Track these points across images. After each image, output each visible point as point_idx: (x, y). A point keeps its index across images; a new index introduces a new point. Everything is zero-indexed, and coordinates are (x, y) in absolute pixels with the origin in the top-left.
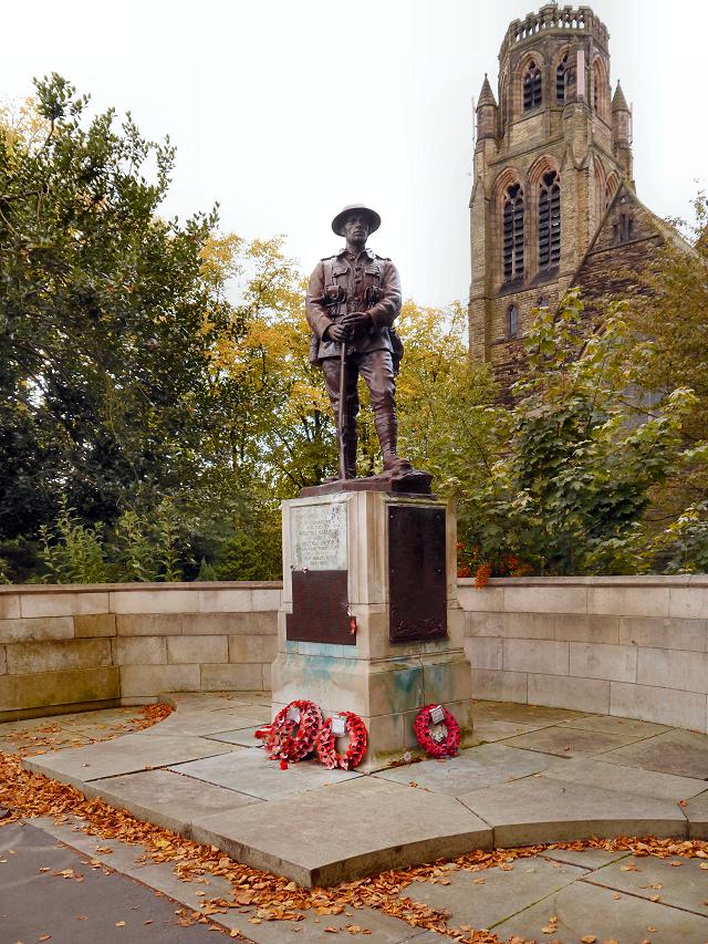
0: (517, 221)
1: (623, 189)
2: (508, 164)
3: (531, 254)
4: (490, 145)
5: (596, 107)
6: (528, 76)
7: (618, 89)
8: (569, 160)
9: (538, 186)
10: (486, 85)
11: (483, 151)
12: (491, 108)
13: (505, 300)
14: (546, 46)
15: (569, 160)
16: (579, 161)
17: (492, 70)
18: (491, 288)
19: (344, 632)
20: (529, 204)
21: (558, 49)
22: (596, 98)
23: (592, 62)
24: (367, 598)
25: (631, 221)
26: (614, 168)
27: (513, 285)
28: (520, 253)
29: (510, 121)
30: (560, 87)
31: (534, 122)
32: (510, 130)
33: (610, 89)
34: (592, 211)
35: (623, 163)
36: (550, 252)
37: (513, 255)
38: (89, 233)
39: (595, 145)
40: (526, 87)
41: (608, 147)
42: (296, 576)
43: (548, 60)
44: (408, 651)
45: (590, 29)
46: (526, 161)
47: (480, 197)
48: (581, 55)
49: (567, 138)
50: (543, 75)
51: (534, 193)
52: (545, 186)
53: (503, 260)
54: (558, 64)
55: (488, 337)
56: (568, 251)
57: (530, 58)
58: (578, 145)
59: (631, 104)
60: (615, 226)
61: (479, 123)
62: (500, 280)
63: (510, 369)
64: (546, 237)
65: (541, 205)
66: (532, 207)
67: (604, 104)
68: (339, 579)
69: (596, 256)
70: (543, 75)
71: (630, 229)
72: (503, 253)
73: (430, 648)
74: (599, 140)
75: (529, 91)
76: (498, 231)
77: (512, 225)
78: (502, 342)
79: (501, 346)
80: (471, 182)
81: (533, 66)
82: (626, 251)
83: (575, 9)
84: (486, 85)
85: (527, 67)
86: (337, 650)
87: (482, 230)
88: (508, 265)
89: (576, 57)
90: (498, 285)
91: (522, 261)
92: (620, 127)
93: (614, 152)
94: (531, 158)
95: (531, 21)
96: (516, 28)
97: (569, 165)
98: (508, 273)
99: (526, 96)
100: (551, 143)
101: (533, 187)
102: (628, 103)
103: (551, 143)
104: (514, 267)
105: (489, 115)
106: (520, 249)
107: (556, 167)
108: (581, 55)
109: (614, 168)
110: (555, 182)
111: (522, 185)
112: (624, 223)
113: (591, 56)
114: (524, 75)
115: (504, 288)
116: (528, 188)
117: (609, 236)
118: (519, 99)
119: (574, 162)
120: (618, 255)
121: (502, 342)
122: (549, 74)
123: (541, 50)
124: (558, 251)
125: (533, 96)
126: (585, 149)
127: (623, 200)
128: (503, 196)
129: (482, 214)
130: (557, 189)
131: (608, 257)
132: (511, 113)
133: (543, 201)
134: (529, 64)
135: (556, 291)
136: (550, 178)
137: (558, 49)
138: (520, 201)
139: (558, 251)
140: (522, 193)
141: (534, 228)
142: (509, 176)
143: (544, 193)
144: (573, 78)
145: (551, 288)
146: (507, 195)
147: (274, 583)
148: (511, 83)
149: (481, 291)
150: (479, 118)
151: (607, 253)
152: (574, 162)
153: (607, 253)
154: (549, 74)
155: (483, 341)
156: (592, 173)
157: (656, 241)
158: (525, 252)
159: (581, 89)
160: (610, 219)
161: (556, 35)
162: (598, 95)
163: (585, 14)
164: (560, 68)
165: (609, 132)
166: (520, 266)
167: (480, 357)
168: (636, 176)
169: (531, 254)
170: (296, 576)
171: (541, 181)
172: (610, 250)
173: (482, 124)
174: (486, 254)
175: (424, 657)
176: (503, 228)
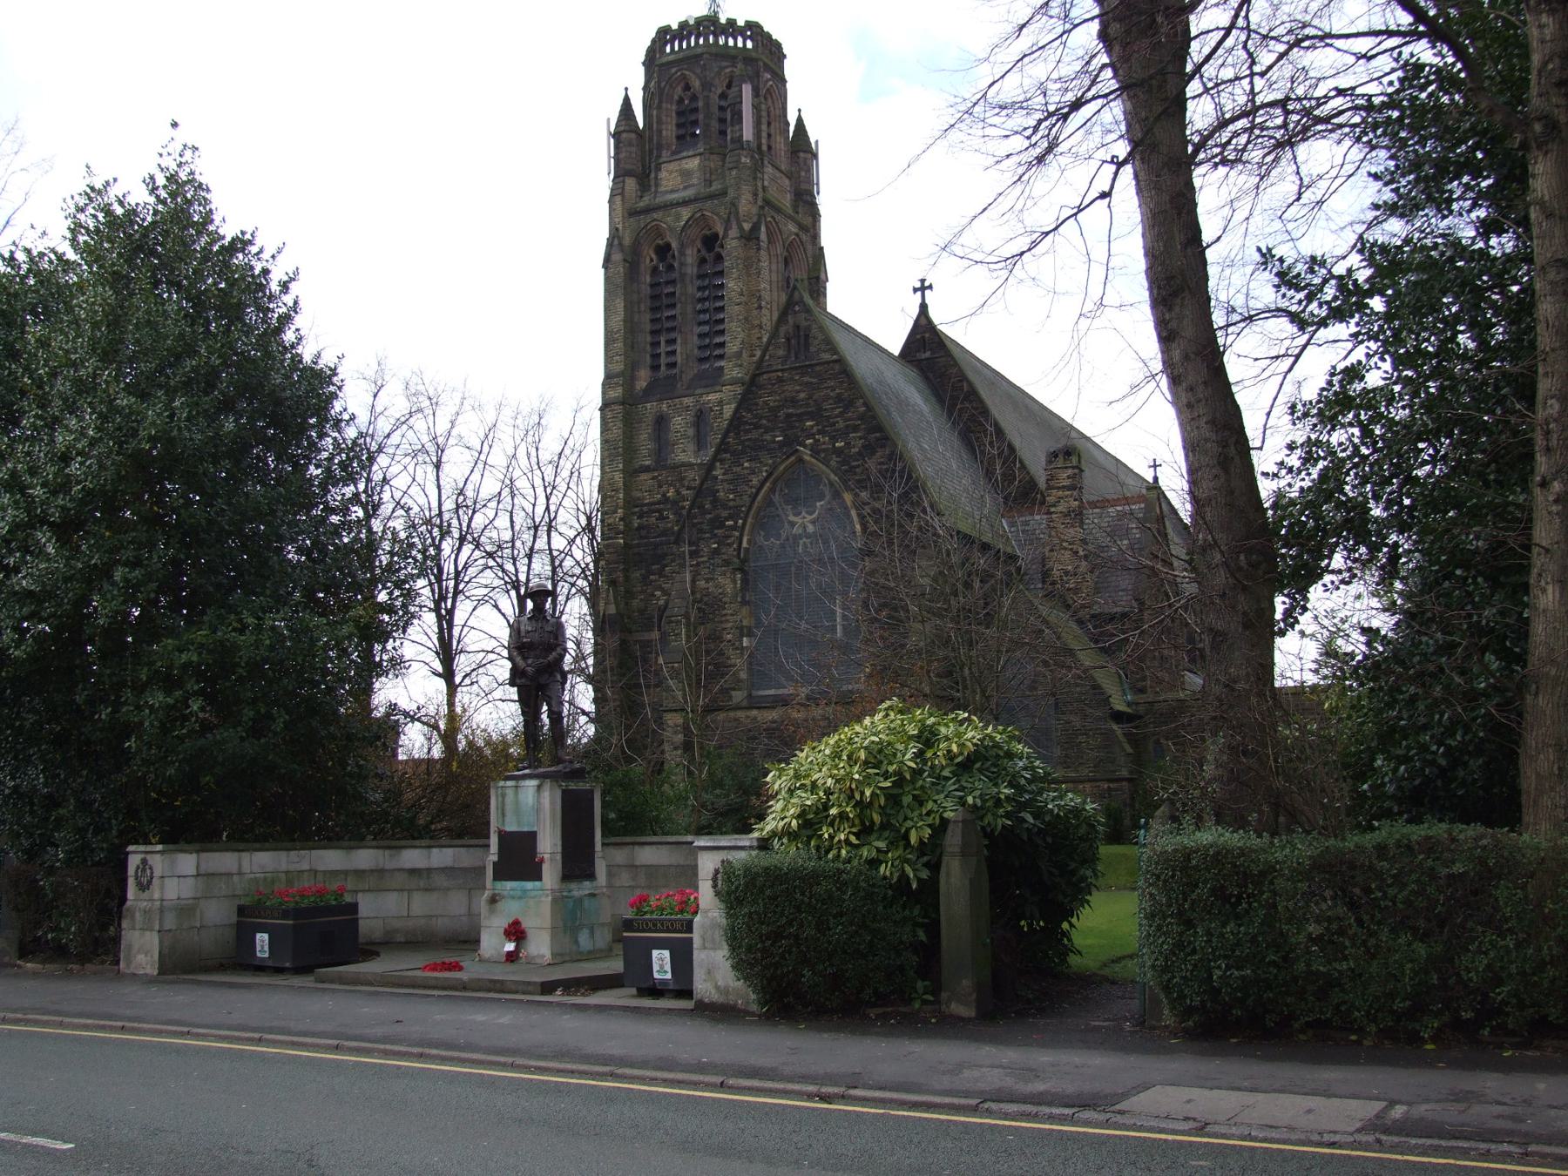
0: (668, 295)
1: (796, 293)
2: (655, 215)
3: (686, 347)
4: (631, 184)
5: (770, 148)
6: (681, 100)
7: (800, 121)
8: (734, 226)
9: (695, 250)
10: (627, 104)
11: (622, 194)
12: (633, 136)
13: (651, 408)
14: (704, 68)
15: (734, 226)
16: (747, 226)
17: (635, 81)
18: (632, 386)
19: (532, 871)
20: (683, 275)
21: (719, 73)
22: (769, 136)
23: (763, 92)
24: (549, 845)
25: (807, 336)
26: (796, 230)
27: (663, 387)
28: (672, 342)
29: (659, 156)
30: (722, 121)
31: (693, 164)
32: (658, 169)
33: (788, 124)
34: (766, 295)
35: (808, 221)
36: (711, 349)
37: (663, 343)
38: (282, 549)
39: (767, 202)
40: (679, 114)
41: (786, 201)
42: (503, 836)
43: (707, 85)
44: (573, 886)
45: (760, 50)
46: (678, 218)
47: (617, 257)
48: (747, 90)
49: (731, 193)
50: (700, 104)
51: (689, 260)
52: (704, 252)
53: (648, 348)
54: (719, 91)
55: (628, 462)
56: (735, 349)
57: (684, 77)
58: (746, 205)
59: (817, 142)
60: (788, 340)
61: (616, 153)
62: (643, 379)
63: (658, 511)
64: (706, 347)
65: (701, 277)
66: (688, 279)
67: (780, 146)
68: (531, 837)
69: (765, 376)
70: (700, 104)
71: (807, 345)
72: (649, 339)
73: (587, 883)
74: (773, 193)
75: (683, 120)
76: (643, 307)
77: (660, 300)
78: (647, 469)
79: (644, 476)
80: (605, 233)
81: (687, 88)
82: (803, 374)
83: (741, 23)
84: (627, 104)
85: (679, 88)
86: (529, 885)
87: (620, 304)
88: (656, 356)
89: (741, 91)
90: (641, 384)
91: (673, 353)
92: (803, 174)
93: (795, 208)
94: (686, 213)
95: (685, 30)
96: (664, 34)
97: (733, 232)
98: (655, 368)
99: (679, 126)
100: (711, 197)
101: (689, 252)
102: (812, 141)
103: (711, 197)
104: (663, 360)
105: (630, 144)
106: (673, 335)
107: (720, 230)
108: (747, 90)
109: (796, 230)
110: (717, 249)
111: (674, 245)
112: (799, 337)
113: (761, 86)
114: (676, 97)
115: (648, 393)
116: (682, 254)
117: (781, 352)
118: (670, 131)
119: (741, 228)
120: (792, 379)
121: (647, 469)
122: (707, 105)
123: (698, 71)
124: (722, 345)
125: (687, 120)
126: (754, 210)
127: (797, 308)
128: (649, 256)
129: (620, 281)
130: (719, 258)
131: (780, 380)
132: (660, 147)
133: (702, 272)
134: (682, 84)
135: (720, 403)
136: (711, 241)
137: (719, 73)
138: (670, 268)
139: (722, 345)
140: (674, 256)
141: (689, 309)
142: (659, 233)
143: (703, 261)
144: (738, 117)
145: (713, 397)
146: (654, 256)
147: (481, 841)
148: (659, 107)
149: (617, 393)
150: (616, 147)
151: (780, 374)
152: (741, 228)
153: (780, 374)
154: (707, 105)
155: (621, 466)
156: (764, 245)
157: (837, 367)
158: (679, 341)
159: (748, 133)
160: (783, 330)
161: (716, 55)
162: (772, 132)
163: (754, 29)
164: (723, 96)
165: (787, 182)
166: (671, 359)
167: (616, 491)
168: (825, 241)
169: (686, 347)
170: (503, 836)
171: (699, 244)
172: (782, 370)
173: (622, 156)
174: (625, 338)
175: (581, 889)
176: (649, 301)
